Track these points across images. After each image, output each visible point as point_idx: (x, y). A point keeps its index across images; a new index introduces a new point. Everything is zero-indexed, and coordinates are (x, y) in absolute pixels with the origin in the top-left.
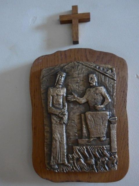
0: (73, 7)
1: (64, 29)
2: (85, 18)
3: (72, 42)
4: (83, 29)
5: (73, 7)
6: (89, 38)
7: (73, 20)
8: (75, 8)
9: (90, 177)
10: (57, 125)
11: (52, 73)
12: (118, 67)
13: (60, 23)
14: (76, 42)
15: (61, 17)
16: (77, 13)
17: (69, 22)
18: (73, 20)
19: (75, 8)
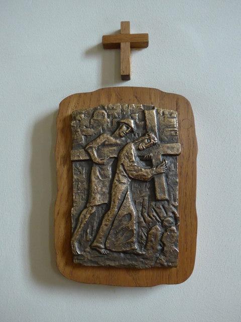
0: (122, 23)
1: (112, 54)
2: (140, 43)
5: (122, 23)
6: (143, 71)
7: (118, 46)
8: (125, 25)
14: (126, 78)
15: (104, 38)
18: (118, 46)
19: (125, 25)
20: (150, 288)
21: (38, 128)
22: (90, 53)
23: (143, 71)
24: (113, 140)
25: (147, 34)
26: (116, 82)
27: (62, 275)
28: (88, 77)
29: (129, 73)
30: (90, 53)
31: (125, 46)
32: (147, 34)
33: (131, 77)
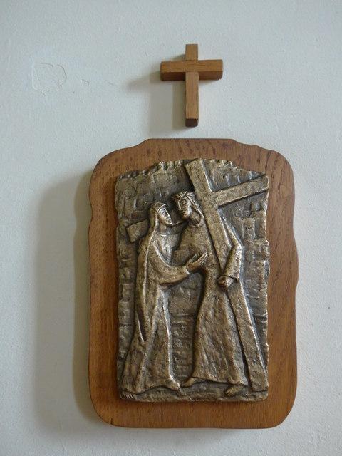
0: (188, 47)
1: (169, 88)
2: (212, 72)
3: (184, 122)
4: (208, 96)
5: (188, 47)
6: (218, 112)
7: (183, 75)
8: (192, 49)
9: (107, 252)
10: (118, 415)
11: (119, 199)
12: (129, 158)
13: (160, 79)
14: (192, 123)
15: (163, 64)
16: (197, 60)
17: (180, 77)
18: (183, 75)
19: (192, 49)
20: (144, 429)
21: (48, 201)
22: (134, 85)
23: (218, 112)
24: (202, 221)
25: (220, 61)
26: (176, 127)
27: (102, 419)
28: (127, 123)
29: (197, 116)
30: (134, 85)
31: (191, 77)
32: (220, 61)
33: (200, 122)
